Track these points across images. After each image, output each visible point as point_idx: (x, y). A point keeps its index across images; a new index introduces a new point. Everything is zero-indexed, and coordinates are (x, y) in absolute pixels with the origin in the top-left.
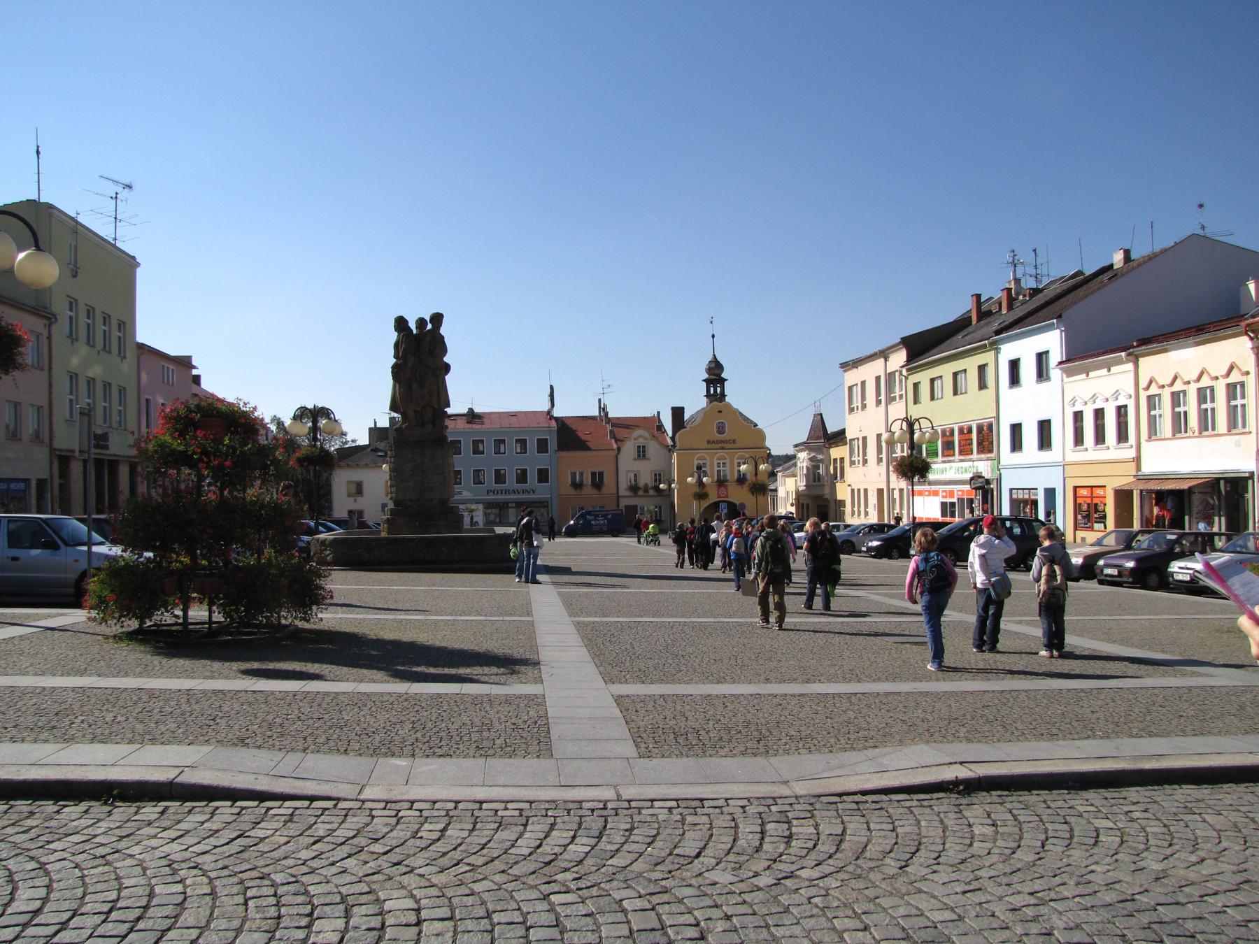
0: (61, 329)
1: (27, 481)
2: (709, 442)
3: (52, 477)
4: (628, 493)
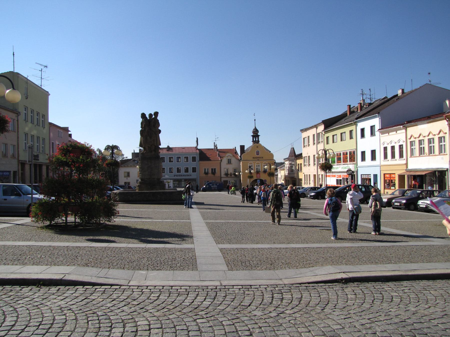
0: (22, 117)
1: (9, 172)
2: (253, 158)
3: (18, 170)
4: (225, 176)
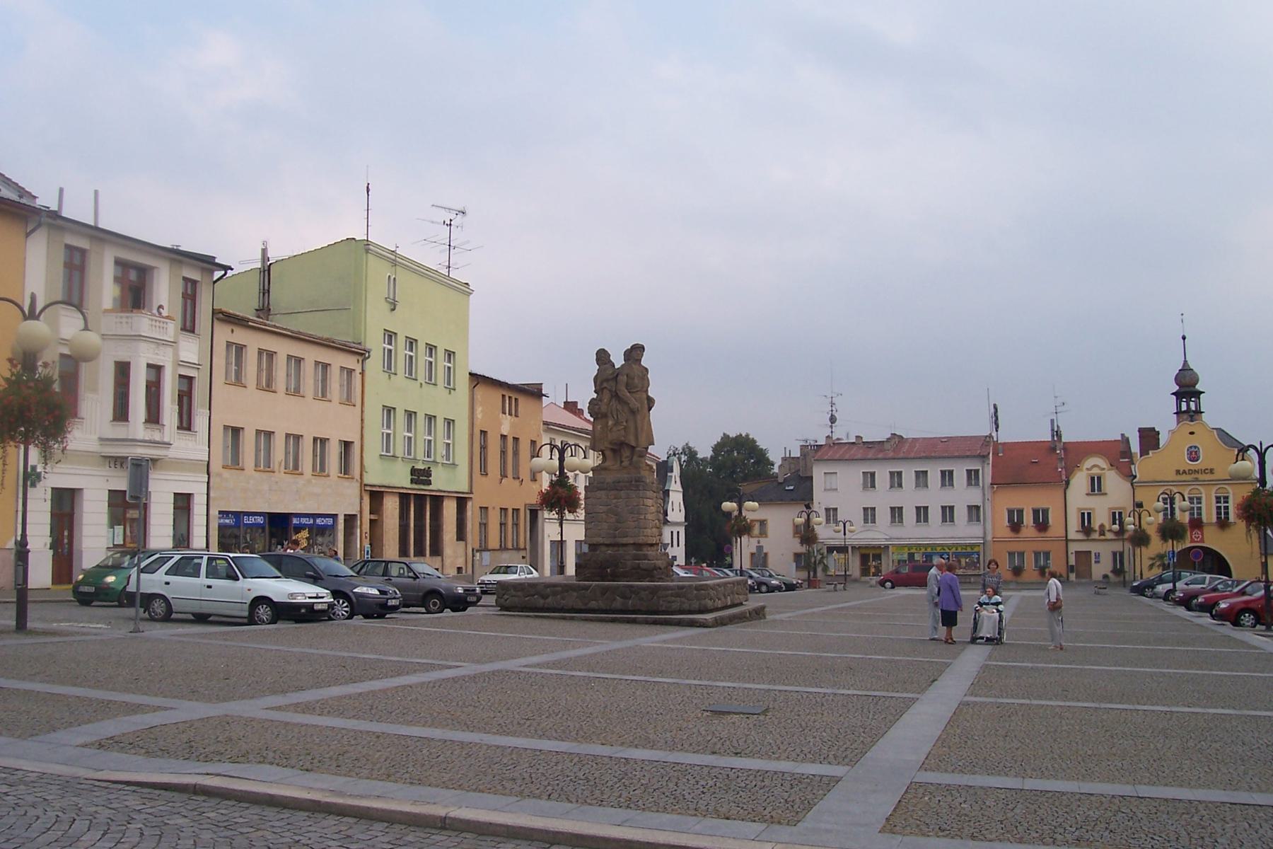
0: (374, 364)
1: (334, 516)
2: (1178, 472)
3: (361, 512)
4: (1080, 536)
